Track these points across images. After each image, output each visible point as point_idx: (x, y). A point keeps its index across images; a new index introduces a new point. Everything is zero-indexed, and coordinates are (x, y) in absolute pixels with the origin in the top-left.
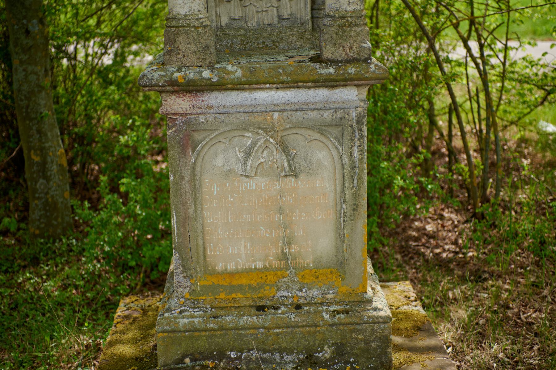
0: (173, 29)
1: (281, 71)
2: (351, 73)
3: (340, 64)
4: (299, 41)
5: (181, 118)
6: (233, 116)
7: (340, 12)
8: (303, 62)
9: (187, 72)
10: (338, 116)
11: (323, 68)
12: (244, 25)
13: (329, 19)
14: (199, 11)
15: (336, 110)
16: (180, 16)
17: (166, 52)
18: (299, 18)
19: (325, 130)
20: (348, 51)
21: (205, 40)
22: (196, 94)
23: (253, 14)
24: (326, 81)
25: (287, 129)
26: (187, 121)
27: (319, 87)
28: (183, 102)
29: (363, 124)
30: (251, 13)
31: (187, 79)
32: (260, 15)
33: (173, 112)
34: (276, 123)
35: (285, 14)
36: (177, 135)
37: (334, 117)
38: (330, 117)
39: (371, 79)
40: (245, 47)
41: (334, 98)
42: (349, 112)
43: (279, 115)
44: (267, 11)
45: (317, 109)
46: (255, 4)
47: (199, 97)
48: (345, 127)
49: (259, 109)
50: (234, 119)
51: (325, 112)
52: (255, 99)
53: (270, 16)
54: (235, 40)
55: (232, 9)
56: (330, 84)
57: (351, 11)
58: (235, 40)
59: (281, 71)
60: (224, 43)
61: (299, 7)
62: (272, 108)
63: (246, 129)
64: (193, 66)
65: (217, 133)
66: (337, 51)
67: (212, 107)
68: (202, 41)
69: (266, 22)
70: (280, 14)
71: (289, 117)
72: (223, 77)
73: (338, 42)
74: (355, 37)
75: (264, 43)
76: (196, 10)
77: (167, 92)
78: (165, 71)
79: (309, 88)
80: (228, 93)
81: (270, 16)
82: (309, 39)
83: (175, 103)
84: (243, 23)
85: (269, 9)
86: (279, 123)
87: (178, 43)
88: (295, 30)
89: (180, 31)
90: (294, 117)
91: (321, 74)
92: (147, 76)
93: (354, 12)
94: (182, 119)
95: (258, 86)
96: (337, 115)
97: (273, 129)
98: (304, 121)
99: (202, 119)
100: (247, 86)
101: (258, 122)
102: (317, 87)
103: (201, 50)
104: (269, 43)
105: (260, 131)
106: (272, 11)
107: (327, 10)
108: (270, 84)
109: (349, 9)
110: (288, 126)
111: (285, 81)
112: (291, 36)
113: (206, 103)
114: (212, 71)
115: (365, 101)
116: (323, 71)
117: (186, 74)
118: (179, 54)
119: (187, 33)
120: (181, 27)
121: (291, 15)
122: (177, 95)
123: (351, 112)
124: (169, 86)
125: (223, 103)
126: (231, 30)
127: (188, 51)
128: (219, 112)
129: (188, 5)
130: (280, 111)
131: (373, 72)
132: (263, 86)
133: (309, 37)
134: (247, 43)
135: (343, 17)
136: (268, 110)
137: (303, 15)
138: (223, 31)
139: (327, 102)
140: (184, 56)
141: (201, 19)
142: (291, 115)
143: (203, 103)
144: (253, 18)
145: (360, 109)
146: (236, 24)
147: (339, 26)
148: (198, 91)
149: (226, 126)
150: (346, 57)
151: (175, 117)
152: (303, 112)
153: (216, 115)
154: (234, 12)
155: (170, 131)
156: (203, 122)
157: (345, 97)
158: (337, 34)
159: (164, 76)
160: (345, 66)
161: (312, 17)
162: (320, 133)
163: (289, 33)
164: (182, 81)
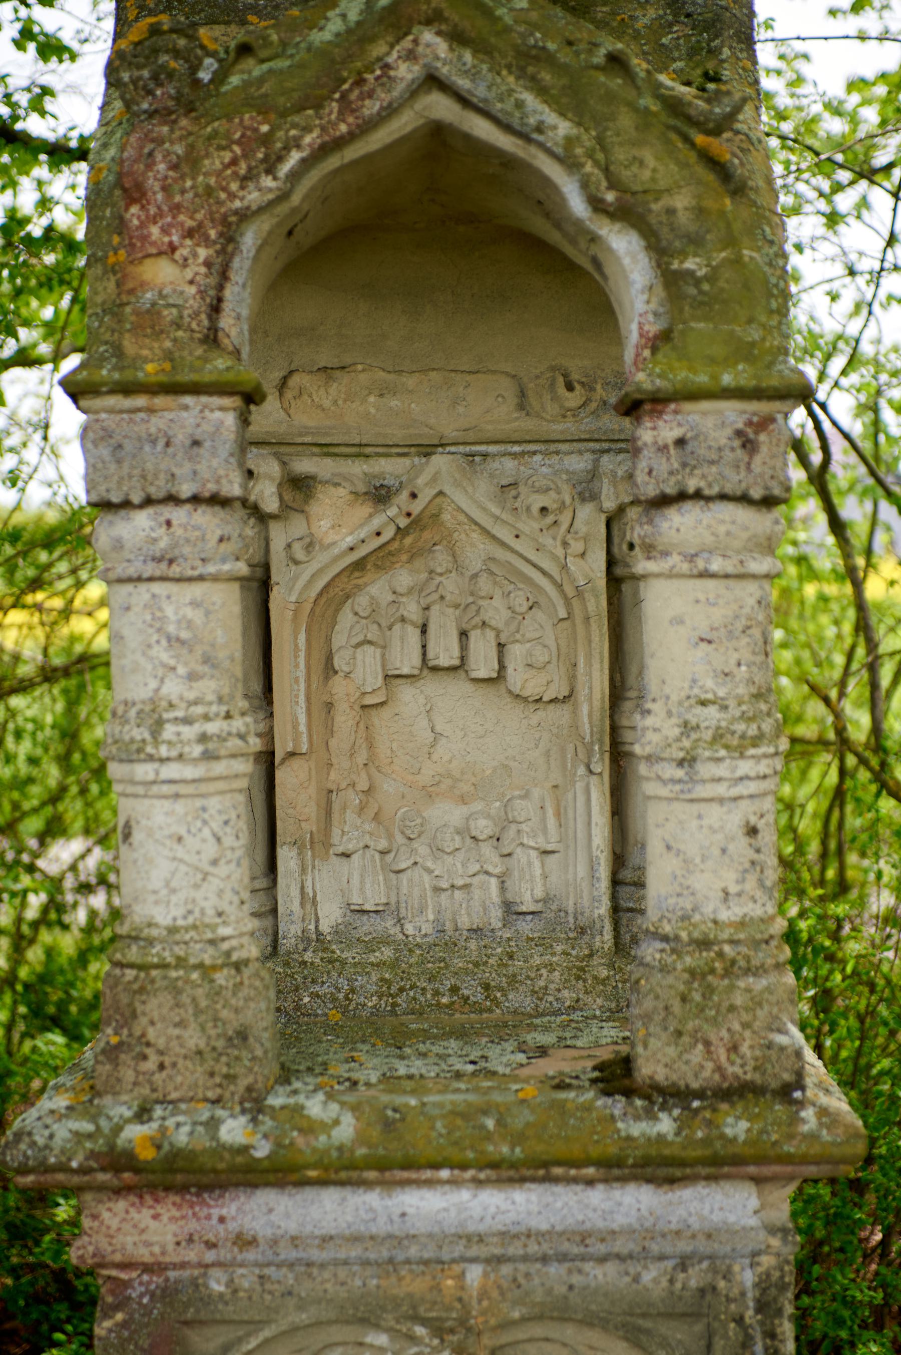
0: (130, 973)
1: (490, 1123)
2: (735, 1139)
3: (696, 1104)
4: (572, 988)
5: (145, 1278)
6: (326, 1275)
7: (695, 926)
8: (569, 1087)
9: (170, 1123)
10: (693, 1283)
11: (637, 1118)
12: (394, 931)
13: (659, 945)
14: (220, 915)
15: (683, 1264)
16: (155, 932)
17: (103, 1052)
18: (571, 910)
19: (647, 1332)
20: (723, 1058)
21: (237, 1011)
22: (198, 1195)
23: (423, 897)
24: (645, 1162)
25: (513, 1323)
26: (164, 1290)
27: (623, 1180)
28: (153, 1224)
29: (779, 1312)
30: (416, 892)
31: (166, 1147)
32: (444, 896)
33: (118, 1258)
34: (474, 1302)
35: (527, 897)
36: (130, 1340)
37: (678, 1285)
38: (664, 1283)
39: (804, 1160)
40: (394, 1005)
41: (676, 1216)
42: (729, 1270)
43: (486, 1275)
44: (466, 886)
45: (618, 1257)
46: (429, 864)
47: (209, 1206)
48: (716, 1325)
49: (413, 1251)
50: (328, 1286)
51: (645, 1267)
52: (403, 1215)
53: (476, 904)
54: (361, 980)
55: (356, 881)
56: (662, 1172)
57: (731, 924)
58: (361, 980)
59: (490, 1123)
60: (325, 989)
61: (570, 876)
62: (459, 1250)
63: (369, 1321)
64: (192, 1099)
65: (267, 1333)
66: (686, 1057)
67: (252, 1242)
68: (225, 1014)
69: (465, 922)
70: (510, 897)
71: (521, 1280)
72: (292, 1144)
73: (690, 1026)
74: (747, 1009)
75: (454, 990)
76: (210, 912)
77: (101, 1188)
78: (94, 1119)
79: (590, 1183)
80: (309, 1193)
81: (476, 904)
82: (604, 982)
83: (127, 1227)
84: (390, 923)
85: (475, 881)
86: (485, 1303)
87: (144, 1021)
88: (559, 948)
89: (153, 981)
90: (537, 1281)
91: (629, 1138)
92: (30, 1134)
93: (742, 924)
94: (149, 1283)
95: (413, 1175)
96: (688, 1278)
97: (463, 1322)
98: (571, 1296)
99: (217, 1285)
100: (372, 1175)
101: (410, 1295)
102: (618, 1179)
103: (220, 1044)
104: (471, 990)
105: (420, 1331)
106: (484, 887)
107: (653, 914)
108: (452, 1168)
109: (724, 915)
110: (516, 1315)
111: (503, 1160)
112: (544, 971)
113: (232, 1226)
114: (254, 1120)
115: (784, 1231)
116: (638, 1129)
117: (163, 1130)
118: (145, 1057)
119: (175, 989)
120: (156, 966)
121: (546, 900)
122: (133, 1198)
123: (736, 1268)
124: (103, 1169)
125: (292, 1227)
126: (349, 947)
127: (178, 1049)
128: (278, 1260)
129: (181, 896)
130: (487, 1261)
131: (813, 1137)
132: (428, 1174)
133: (604, 973)
134: (402, 990)
135: (704, 944)
136: (446, 1257)
137: (586, 902)
138: (325, 950)
139: (651, 1234)
140: (162, 1067)
141: (224, 939)
142: (527, 1275)
143: (221, 1228)
144: (422, 910)
145: (767, 1261)
146: (366, 927)
147: (692, 972)
148: (209, 1188)
149: (301, 1307)
150: (717, 1077)
151: (124, 1276)
152: (567, 1265)
153: (267, 1271)
154: (362, 890)
155: (107, 1324)
156: (221, 1295)
157: (717, 1217)
158: (684, 999)
159: (90, 1136)
160: (715, 1110)
161: (616, 909)
162: (627, 1339)
163: (537, 961)
164: (147, 1154)
